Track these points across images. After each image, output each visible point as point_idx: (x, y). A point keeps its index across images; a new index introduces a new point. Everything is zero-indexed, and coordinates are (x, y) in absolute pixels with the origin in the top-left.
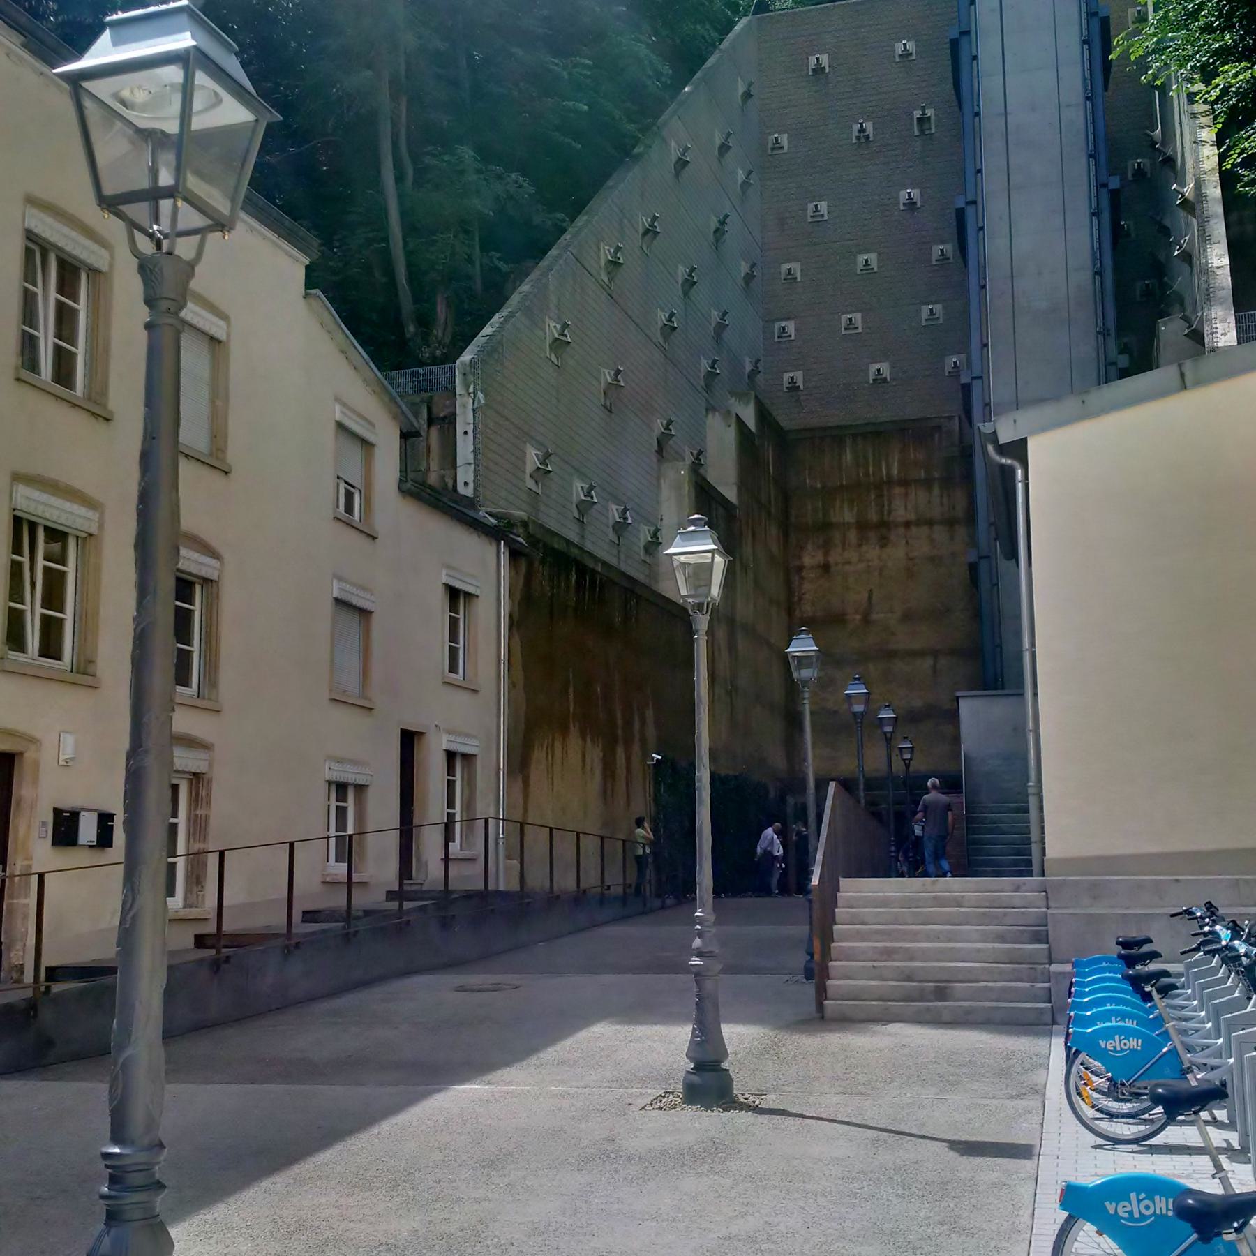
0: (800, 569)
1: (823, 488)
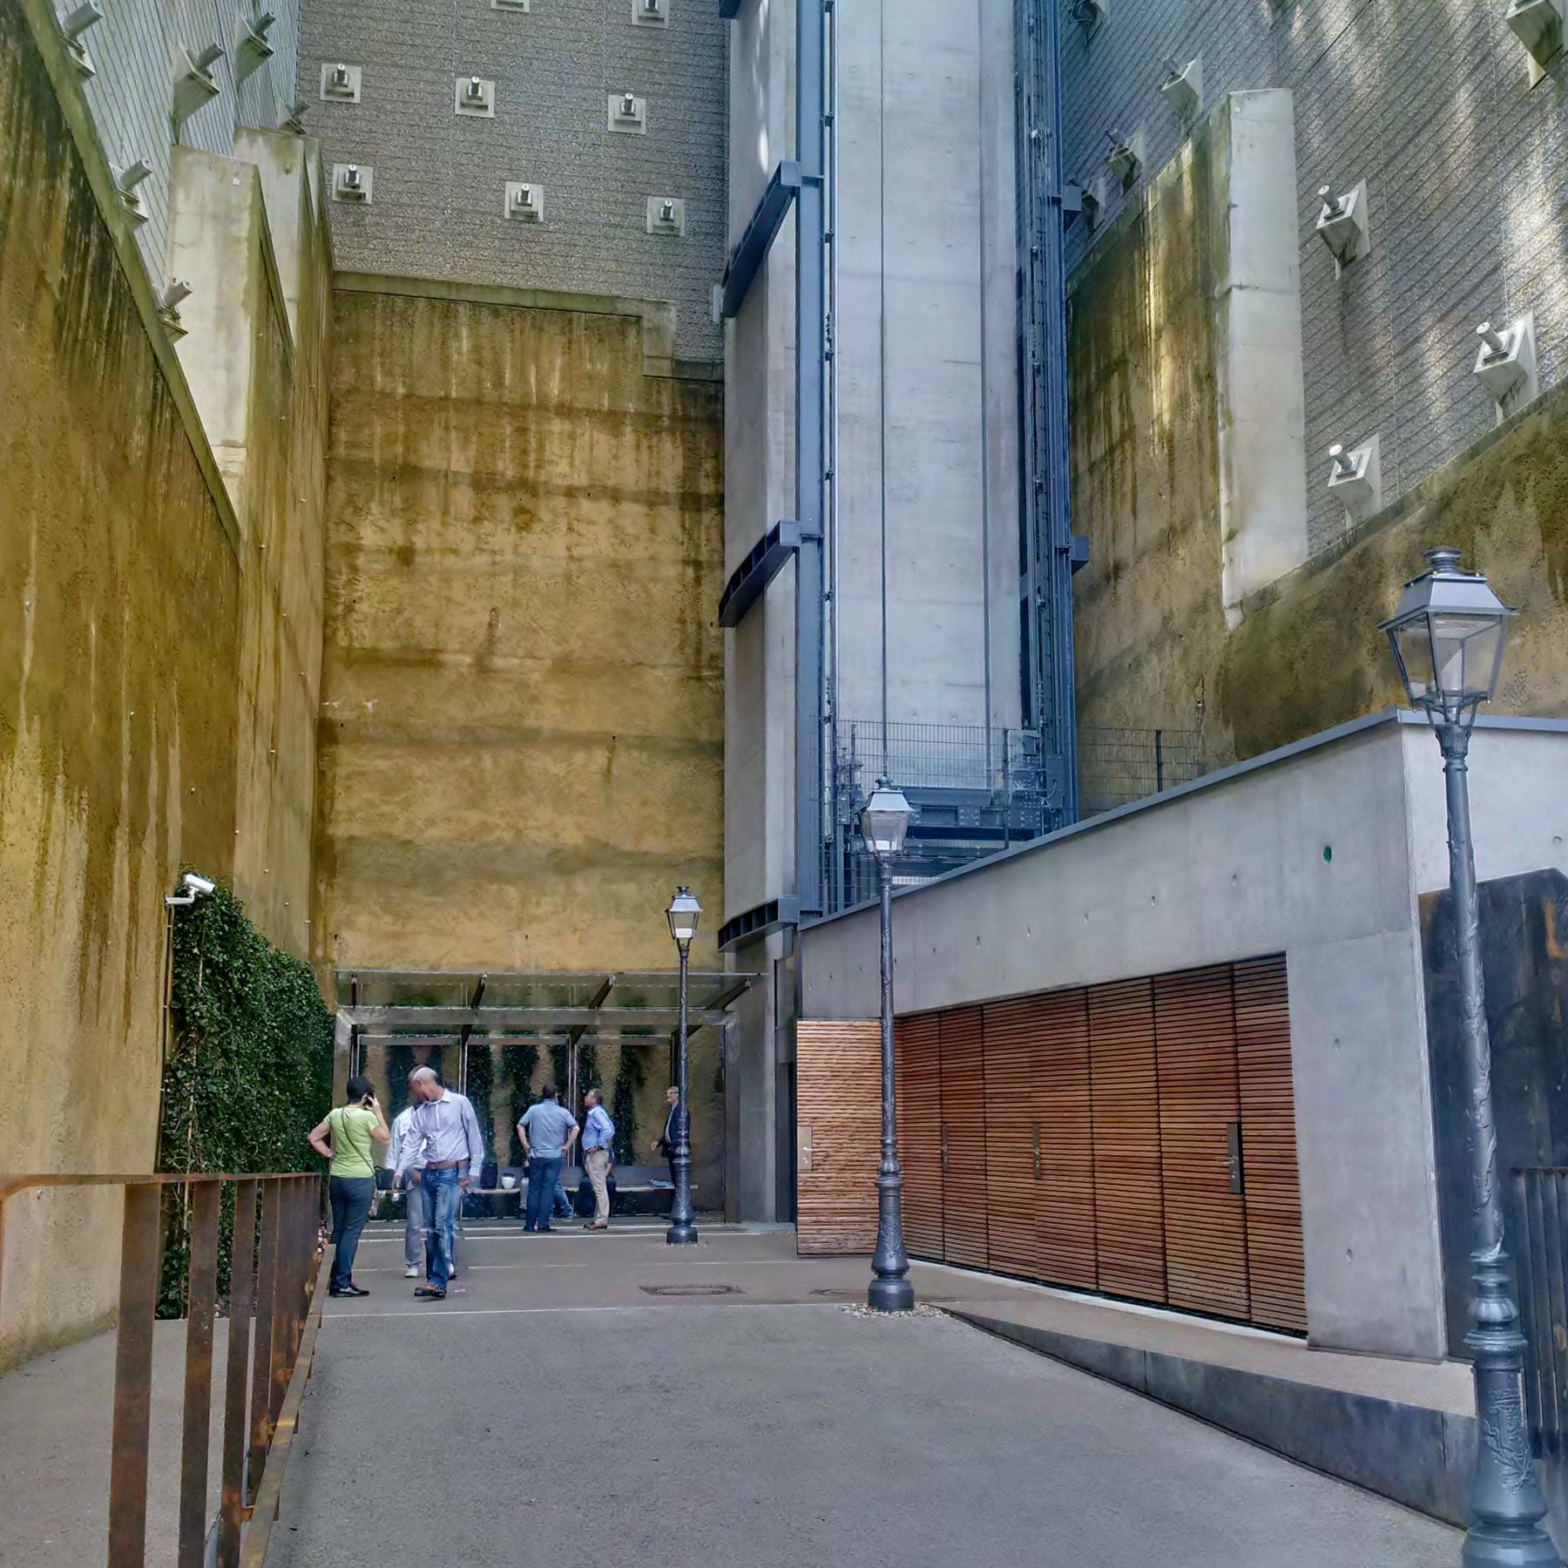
0: (352, 549)
1: (408, 396)
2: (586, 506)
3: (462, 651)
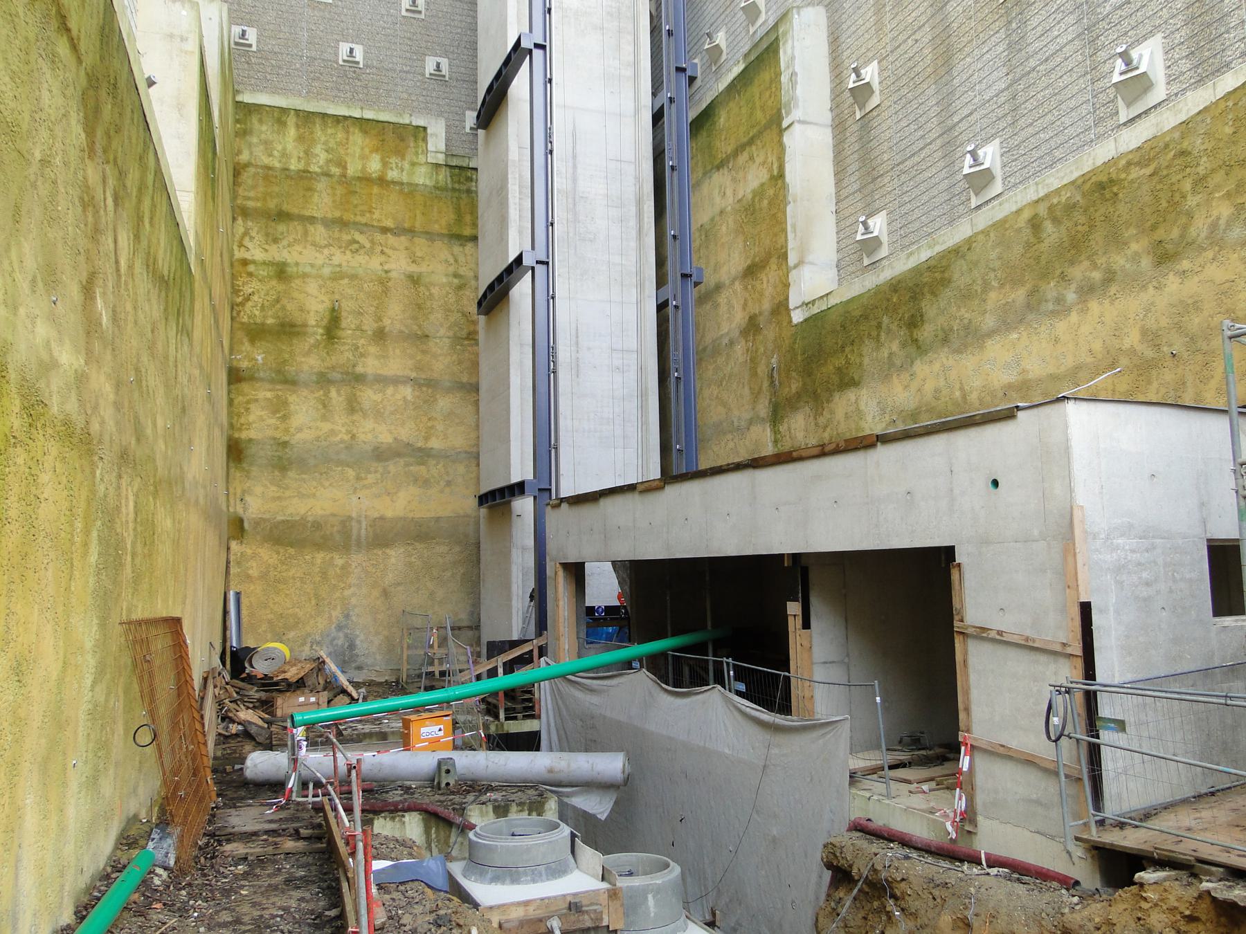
2: (391, 239)
3: (317, 326)
